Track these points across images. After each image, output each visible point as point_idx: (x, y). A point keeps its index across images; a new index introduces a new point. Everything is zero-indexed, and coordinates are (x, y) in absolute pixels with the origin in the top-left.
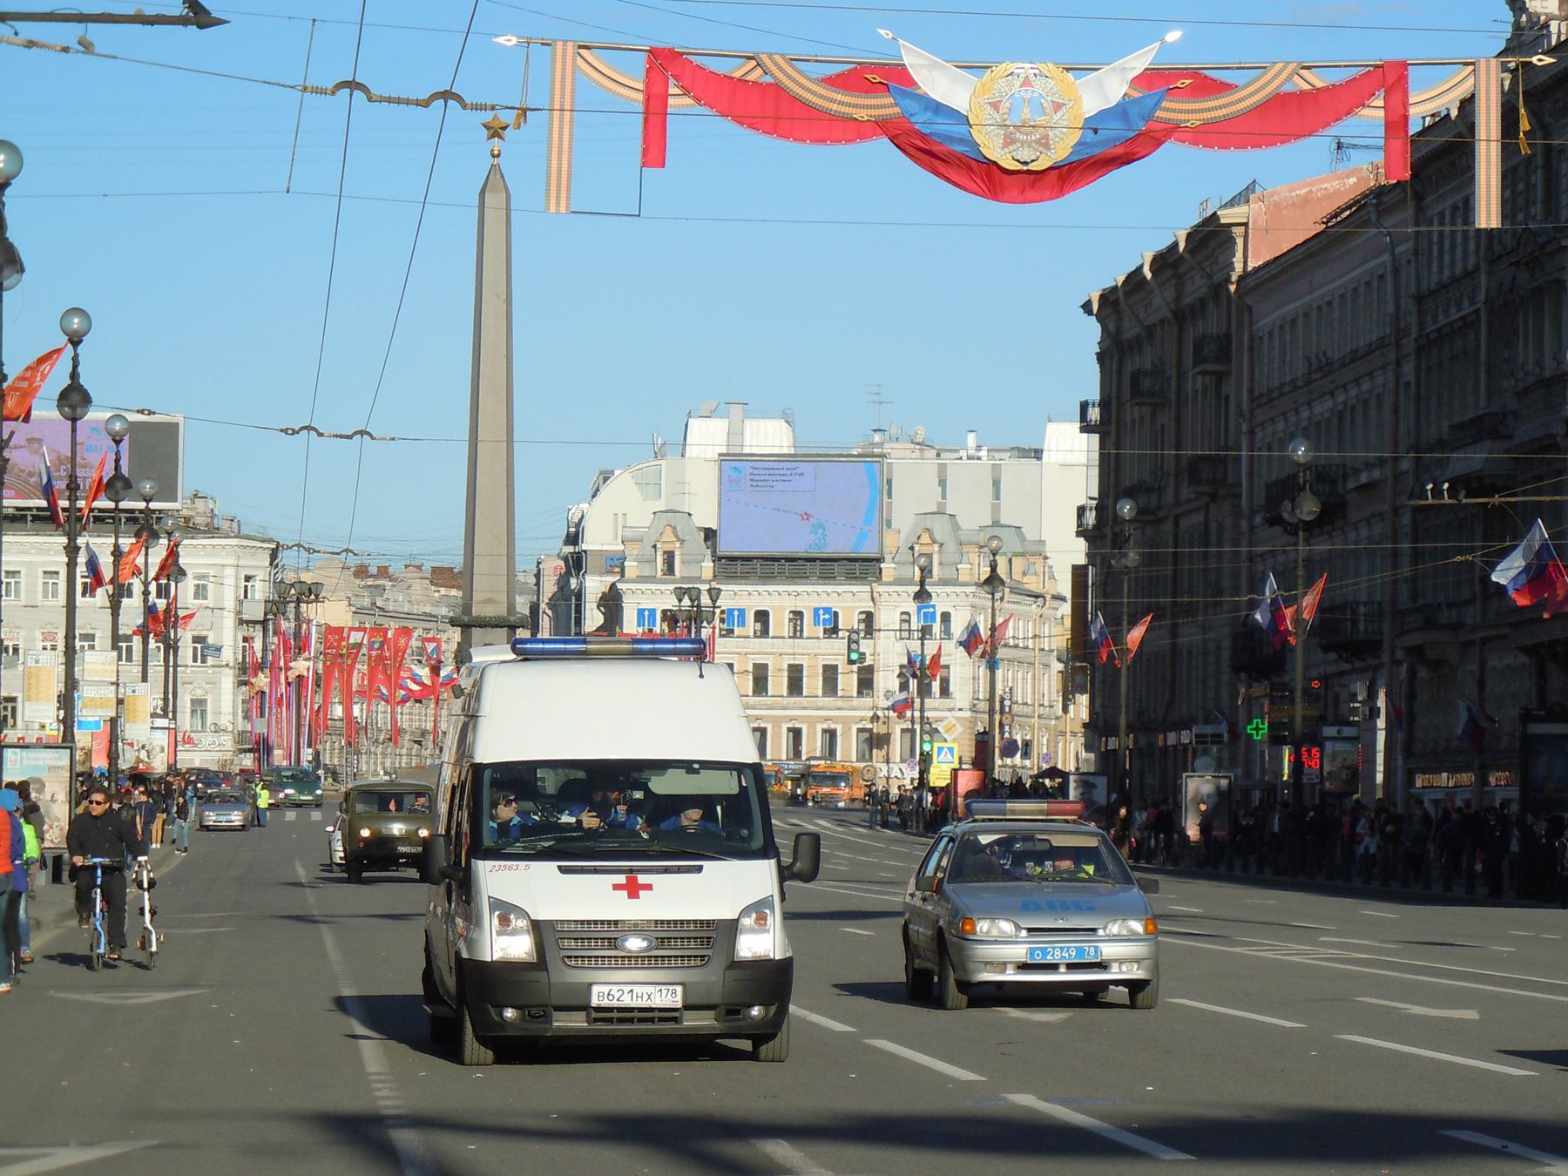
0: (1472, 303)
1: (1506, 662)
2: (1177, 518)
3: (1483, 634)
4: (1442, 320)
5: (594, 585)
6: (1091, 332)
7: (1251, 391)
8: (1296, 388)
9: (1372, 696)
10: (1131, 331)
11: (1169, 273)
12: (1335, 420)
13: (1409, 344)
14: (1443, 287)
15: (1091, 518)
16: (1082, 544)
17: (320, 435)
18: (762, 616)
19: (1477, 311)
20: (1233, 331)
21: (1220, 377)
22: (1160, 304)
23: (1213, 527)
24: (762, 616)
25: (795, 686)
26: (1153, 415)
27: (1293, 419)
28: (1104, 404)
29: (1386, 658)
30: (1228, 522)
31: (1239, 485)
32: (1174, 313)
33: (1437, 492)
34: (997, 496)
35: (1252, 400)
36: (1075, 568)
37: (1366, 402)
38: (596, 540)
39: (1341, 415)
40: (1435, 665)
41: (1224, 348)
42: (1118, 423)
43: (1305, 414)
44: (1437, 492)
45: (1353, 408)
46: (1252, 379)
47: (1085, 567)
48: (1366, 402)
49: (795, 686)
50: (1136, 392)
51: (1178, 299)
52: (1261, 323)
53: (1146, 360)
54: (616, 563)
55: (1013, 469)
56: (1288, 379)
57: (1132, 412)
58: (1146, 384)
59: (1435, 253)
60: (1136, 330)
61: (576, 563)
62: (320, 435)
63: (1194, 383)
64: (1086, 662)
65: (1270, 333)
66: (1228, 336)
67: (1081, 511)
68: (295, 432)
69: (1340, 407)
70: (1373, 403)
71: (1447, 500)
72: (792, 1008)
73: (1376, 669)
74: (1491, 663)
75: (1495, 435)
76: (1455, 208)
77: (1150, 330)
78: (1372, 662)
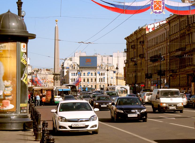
0: (177, 36)
1: (185, 76)
2: (137, 61)
3: (180, 73)
4: (173, 38)
5: (65, 70)
6: (126, 41)
7: (147, 47)
8: (153, 46)
9: (164, 80)
10: (130, 41)
11: (136, 34)
12: (158, 50)
13: (168, 41)
14: (173, 34)
15: (126, 62)
16: (125, 65)
17: (84, 43)
18: (92, 73)
19: (178, 37)
20: (144, 40)
21: (143, 46)
22: (134, 38)
23: (142, 62)
24: (92, 73)
25: (88, 81)
26: (134, 50)
27: (153, 50)
28: (127, 49)
29: (166, 76)
30: (144, 62)
31: (145, 57)
32: (136, 39)
33: (186, 56)
34: (108, 60)
35: (147, 48)
36: (124, 67)
37: (162, 48)
38: (65, 66)
39: (159, 49)
40: (173, 77)
41: (143, 42)
42: (129, 51)
43: (154, 49)
44: (186, 56)
45: (161, 48)
46: (147, 46)
47: (125, 67)
48: (162, 48)
49: (88, 81)
50: (132, 47)
51: (137, 37)
52: (148, 39)
53: (133, 44)
54: (68, 68)
55: (110, 58)
56: (152, 45)
57: (131, 50)
58: (133, 47)
59: (172, 31)
60: (131, 41)
61: (63, 68)
62: (84, 43)
63: (139, 46)
64: (126, 77)
65: (149, 41)
66: (144, 41)
67: (125, 61)
68: (80, 43)
69: (159, 48)
70: (164, 48)
71: (187, 57)
72: (194, 128)
73: (164, 77)
74: (171, 78)
75: (182, 50)
76: (175, 25)
77: (133, 41)
78: (164, 76)
